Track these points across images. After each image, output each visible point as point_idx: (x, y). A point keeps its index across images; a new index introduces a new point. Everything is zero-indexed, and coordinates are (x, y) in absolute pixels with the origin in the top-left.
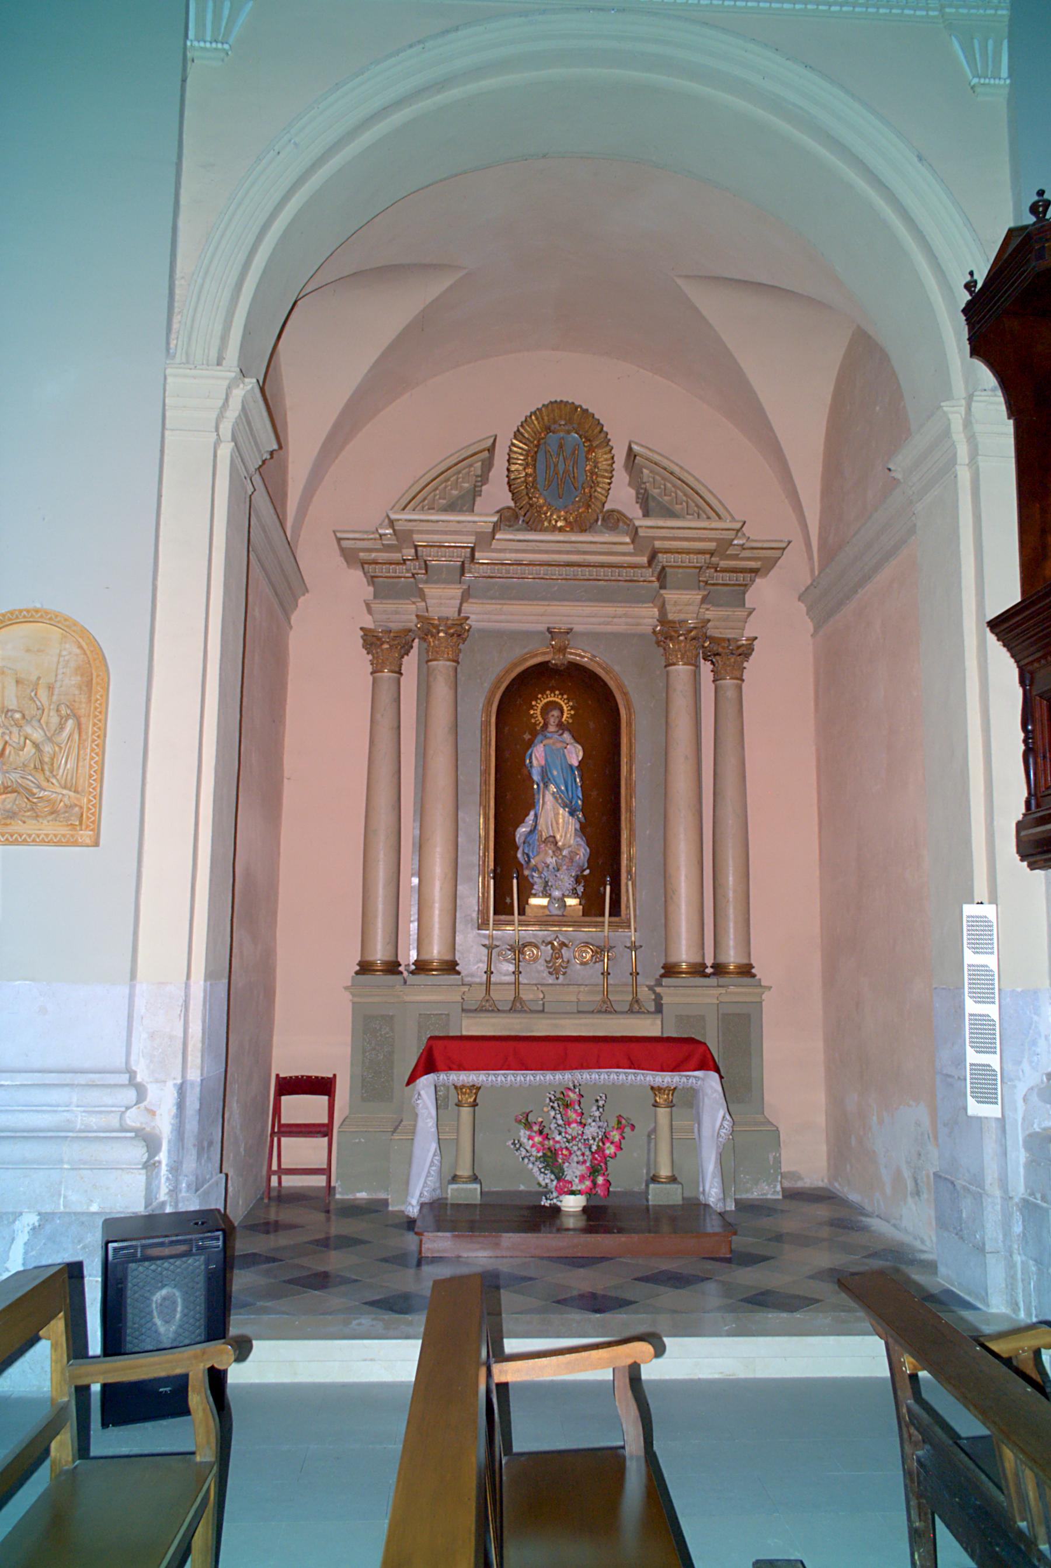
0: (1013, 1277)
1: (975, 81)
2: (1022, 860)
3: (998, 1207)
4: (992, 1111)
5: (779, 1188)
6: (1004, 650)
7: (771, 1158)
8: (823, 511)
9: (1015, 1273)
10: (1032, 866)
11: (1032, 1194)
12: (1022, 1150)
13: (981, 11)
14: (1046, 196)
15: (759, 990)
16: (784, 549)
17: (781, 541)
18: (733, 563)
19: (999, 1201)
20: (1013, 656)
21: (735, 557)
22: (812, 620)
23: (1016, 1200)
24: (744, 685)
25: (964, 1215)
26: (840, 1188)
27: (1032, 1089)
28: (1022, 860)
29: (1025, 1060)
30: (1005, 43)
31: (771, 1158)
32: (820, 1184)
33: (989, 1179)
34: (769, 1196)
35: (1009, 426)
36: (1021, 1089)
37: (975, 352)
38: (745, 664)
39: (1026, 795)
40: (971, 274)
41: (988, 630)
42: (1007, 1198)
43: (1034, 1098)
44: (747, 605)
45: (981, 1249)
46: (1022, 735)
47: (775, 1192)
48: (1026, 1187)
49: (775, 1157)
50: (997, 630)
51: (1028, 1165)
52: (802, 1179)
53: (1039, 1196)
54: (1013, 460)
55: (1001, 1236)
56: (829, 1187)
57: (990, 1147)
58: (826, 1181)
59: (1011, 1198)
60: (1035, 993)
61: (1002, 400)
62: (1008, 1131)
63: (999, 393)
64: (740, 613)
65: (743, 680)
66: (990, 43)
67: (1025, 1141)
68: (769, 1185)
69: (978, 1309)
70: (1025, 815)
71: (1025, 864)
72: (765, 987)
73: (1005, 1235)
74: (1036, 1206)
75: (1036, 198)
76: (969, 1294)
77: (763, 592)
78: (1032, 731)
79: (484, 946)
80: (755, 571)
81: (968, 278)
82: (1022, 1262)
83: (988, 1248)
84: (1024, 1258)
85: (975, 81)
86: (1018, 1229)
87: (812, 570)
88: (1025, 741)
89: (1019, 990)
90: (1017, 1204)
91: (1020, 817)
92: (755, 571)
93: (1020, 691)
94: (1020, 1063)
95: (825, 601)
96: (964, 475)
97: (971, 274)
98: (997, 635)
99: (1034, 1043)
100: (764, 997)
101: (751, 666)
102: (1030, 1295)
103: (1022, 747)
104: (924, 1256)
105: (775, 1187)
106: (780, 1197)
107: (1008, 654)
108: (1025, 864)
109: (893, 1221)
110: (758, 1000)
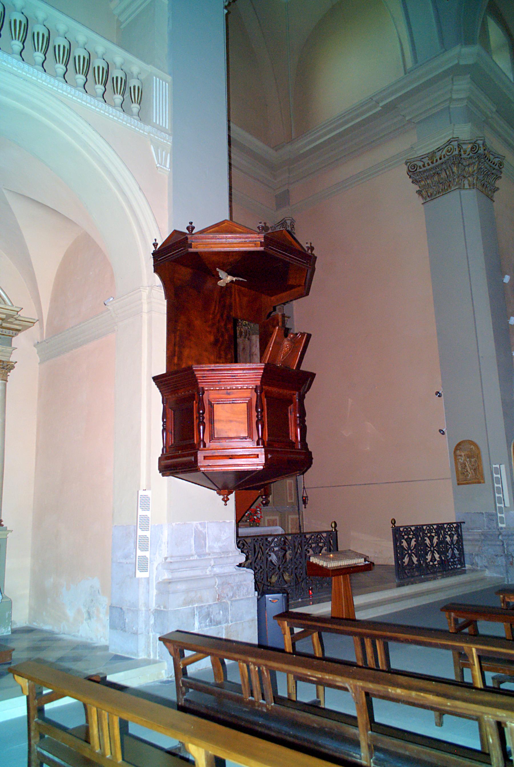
0: (149, 643)
1: (158, 165)
2: (160, 472)
3: (143, 615)
4: (145, 575)
5: (10, 629)
6: (157, 389)
7: (7, 615)
8: (50, 308)
9: (150, 640)
10: (163, 475)
11: (159, 606)
12: (155, 589)
13: (162, 140)
14: (193, 225)
15: (6, 532)
16: (34, 323)
17: (34, 319)
18: (9, 325)
19: (144, 612)
20: (160, 392)
21: (11, 323)
22: (39, 356)
23: (152, 610)
24: (7, 383)
25: (127, 621)
26: (35, 625)
27: (159, 564)
28: (160, 472)
29: (157, 553)
30: (169, 155)
31: (7, 615)
32: (24, 625)
33: (140, 604)
34: (5, 634)
35: (165, 302)
36: (156, 564)
37: (155, 271)
38: (9, 374)
39: (162, 447)
40: (156, 240)
41: (152, 380)
42: (148, 610)
43: (160, 568)
44: (13, 346)
45: (136, 633)
46: (162, 423)
47: (8, 632)
48: (156, 604)
49: (9, 614)
50: (157, 381)
51: (156, 595)
52: (16, 624)
53: (162, 607)
54: (166, 316)
55: (144, 627)
56: (29, 625)
57: (142, 590)
58: (27, 623)
59: (150, 610)
60: (162, 525)
61: (163, 291)
62: (150, 582)
63: (162, 288)
64: (9, 349)
65: (7, 381)
66: (164, 153)
67: (156, 586)
68: (5, 628)
69: (133, 659)
70: (162, 455)
71: (161, 474)
72: (9, 531)
73: (146, 626)
74: (162, 611)
75: (189, 225)
76: (128, 654)
77: (20, 341)
78: (166, 422)
79: (305, 508)
80: (19, 330)
81: (154, 241)
82: (153, 635)
83: (139, 632)
84: (154, 633)
85: (158, 165)
86: (152, 622)
87: (42, 334)
88: (163, 426)
89: (156, 525)
90: (152, 612)
91: (160, 456)
92: (19, 330)
93: (162, 406)
94: (155, 554)
95: (48, 351)
96: (145, 317)
97: (156, 240)
98: (155, 382)
99: (160, 546)
100: (8, 535)
101: (12, 374)
102: (156, 648)
103: (162, 428)
104: (96, 645)
105: (8, 628)
106: (10, 633)
107: (159, 391)
108: (161, 474)
109: (73, 634)
110: (5, 537)
